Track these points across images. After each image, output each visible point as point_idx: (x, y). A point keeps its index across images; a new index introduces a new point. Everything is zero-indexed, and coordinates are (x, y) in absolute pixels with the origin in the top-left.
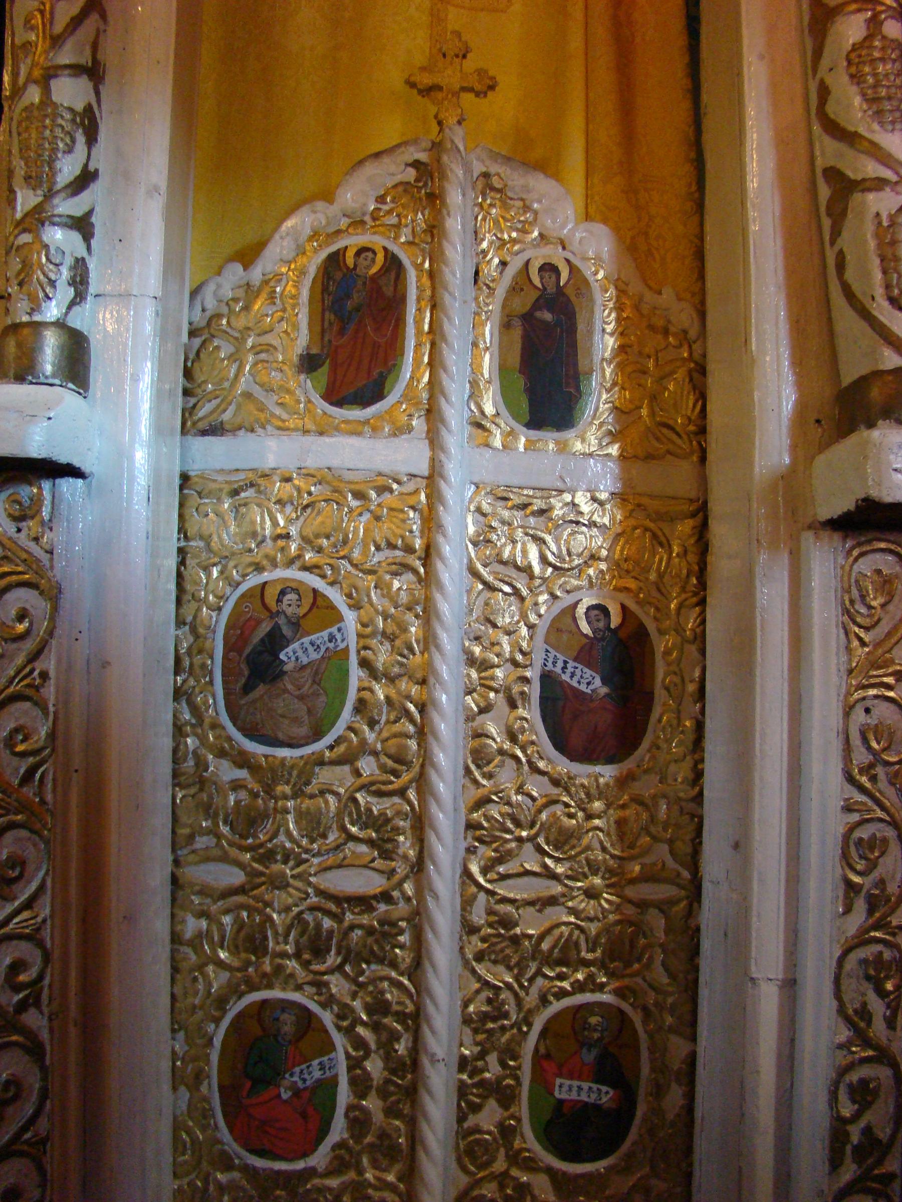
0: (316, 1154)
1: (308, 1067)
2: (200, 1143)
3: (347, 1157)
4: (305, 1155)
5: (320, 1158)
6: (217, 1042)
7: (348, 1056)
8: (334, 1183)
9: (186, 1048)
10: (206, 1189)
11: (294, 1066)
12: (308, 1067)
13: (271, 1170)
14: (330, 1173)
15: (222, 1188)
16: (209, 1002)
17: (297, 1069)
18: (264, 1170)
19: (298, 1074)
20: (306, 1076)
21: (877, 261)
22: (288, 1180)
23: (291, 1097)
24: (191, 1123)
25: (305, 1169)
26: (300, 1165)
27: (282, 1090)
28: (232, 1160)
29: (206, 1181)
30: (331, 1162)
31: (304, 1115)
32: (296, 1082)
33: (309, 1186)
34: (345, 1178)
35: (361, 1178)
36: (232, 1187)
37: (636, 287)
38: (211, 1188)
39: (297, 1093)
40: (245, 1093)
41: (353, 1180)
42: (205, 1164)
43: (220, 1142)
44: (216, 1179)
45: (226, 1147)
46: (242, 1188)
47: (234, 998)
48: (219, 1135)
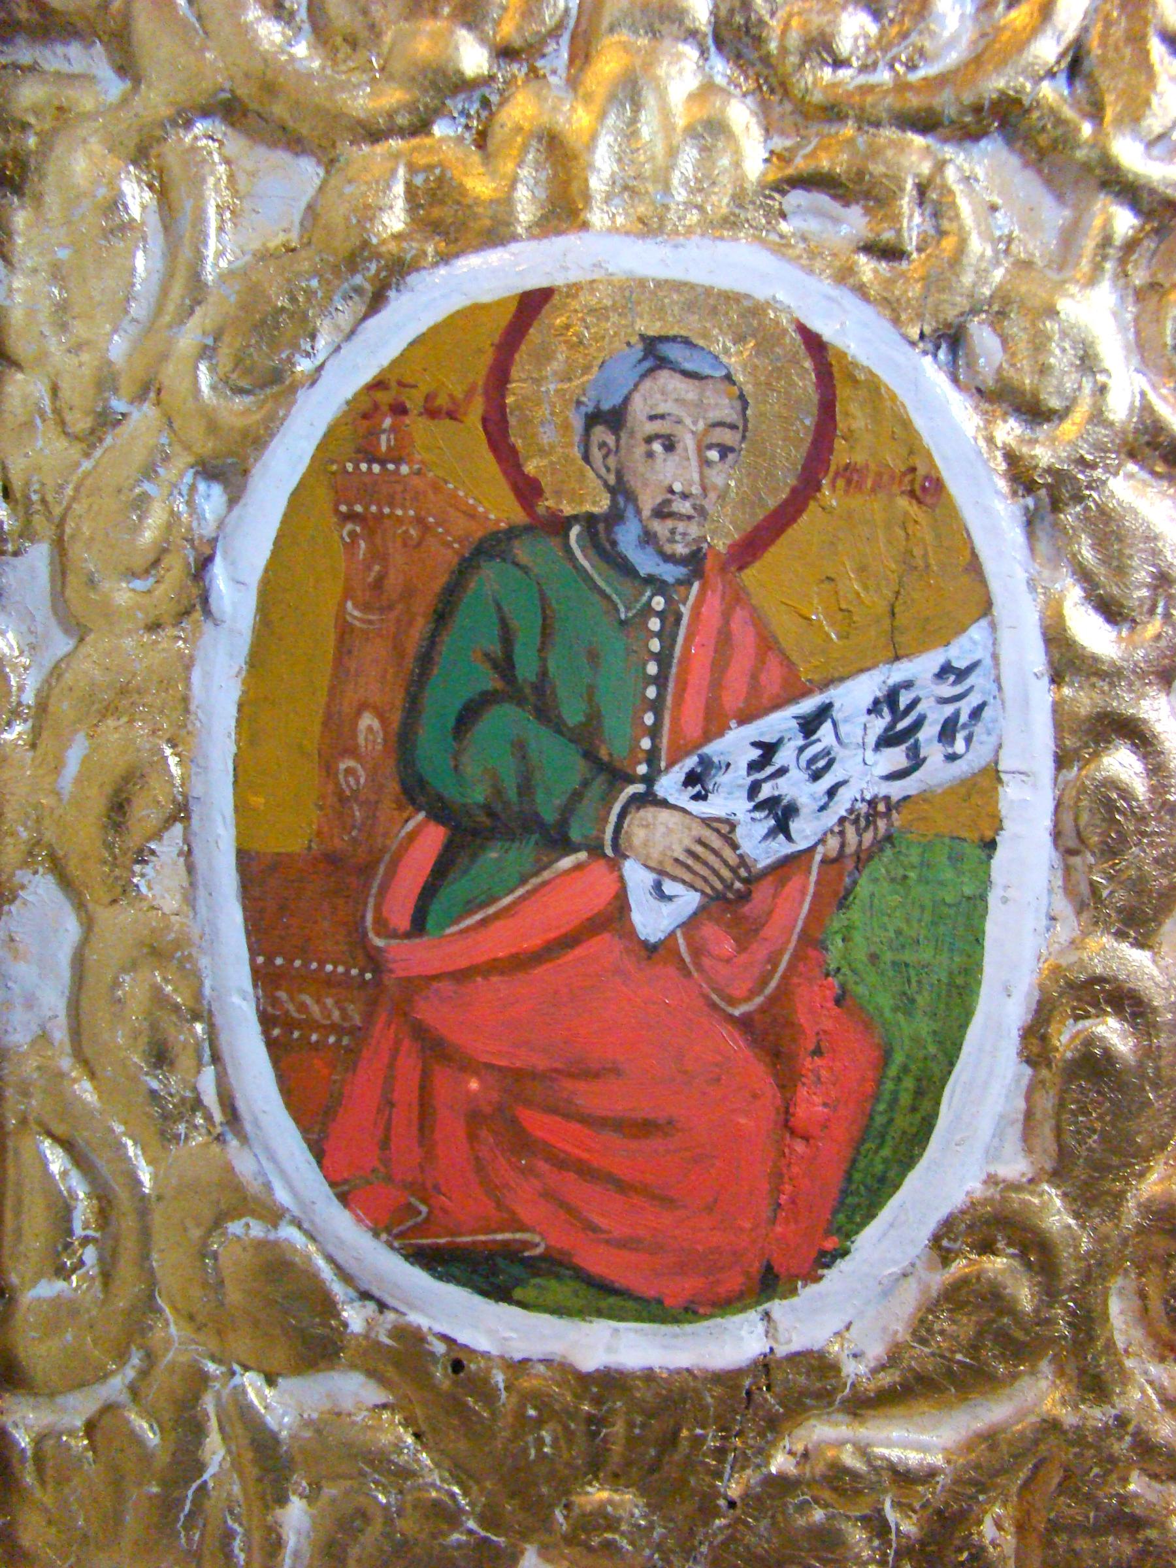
0: (836, 1277)
1: (809, 726)
2: (143, 1207)
3: (1025, 1295)
4: (769, 1284)
5: (857, 1303)
6: (235, 590)
7: (1065, 660)
8: (919, 1441)
9: (62, 644)
10: (187, 1463)
11: (714, 728)
12: (809, 726)
13: (563, 1370)
14: (908, 1387)
15: (271, 1463)
16: (189, 338)
17: (735, 745)
18: (518, 1367)
19: (739, 775)
20: (795, 787)
21: (931, 372)
22: (659, 1429)
23: (690, 924)
24: (86, 1091)
25: (765, 1366)
26: (734, 1342)
27: (637, 877)
28: (328, 1307)
29: (188, 1427)
30: (922, 1330)
31: (771, 1037)
32: (726, 828)
33: (780, 1463)
34: (995, 1412)
35: (1097, 1415)
36: (334, 1453)
37: (746, 303)
38: (215, 1452)
39: (733, 898)
40: (400, 915)
41: (1052, 1426)
42: (172, 1332)
43: (240, 1201)
44: (244, 1414)
45: (288, 1232)
46: (381, 1463)
47: (346, 312)
48: (245, 1164)
